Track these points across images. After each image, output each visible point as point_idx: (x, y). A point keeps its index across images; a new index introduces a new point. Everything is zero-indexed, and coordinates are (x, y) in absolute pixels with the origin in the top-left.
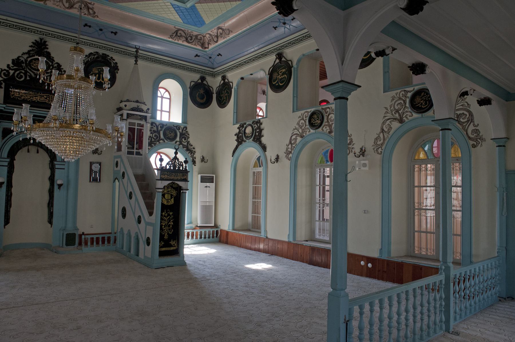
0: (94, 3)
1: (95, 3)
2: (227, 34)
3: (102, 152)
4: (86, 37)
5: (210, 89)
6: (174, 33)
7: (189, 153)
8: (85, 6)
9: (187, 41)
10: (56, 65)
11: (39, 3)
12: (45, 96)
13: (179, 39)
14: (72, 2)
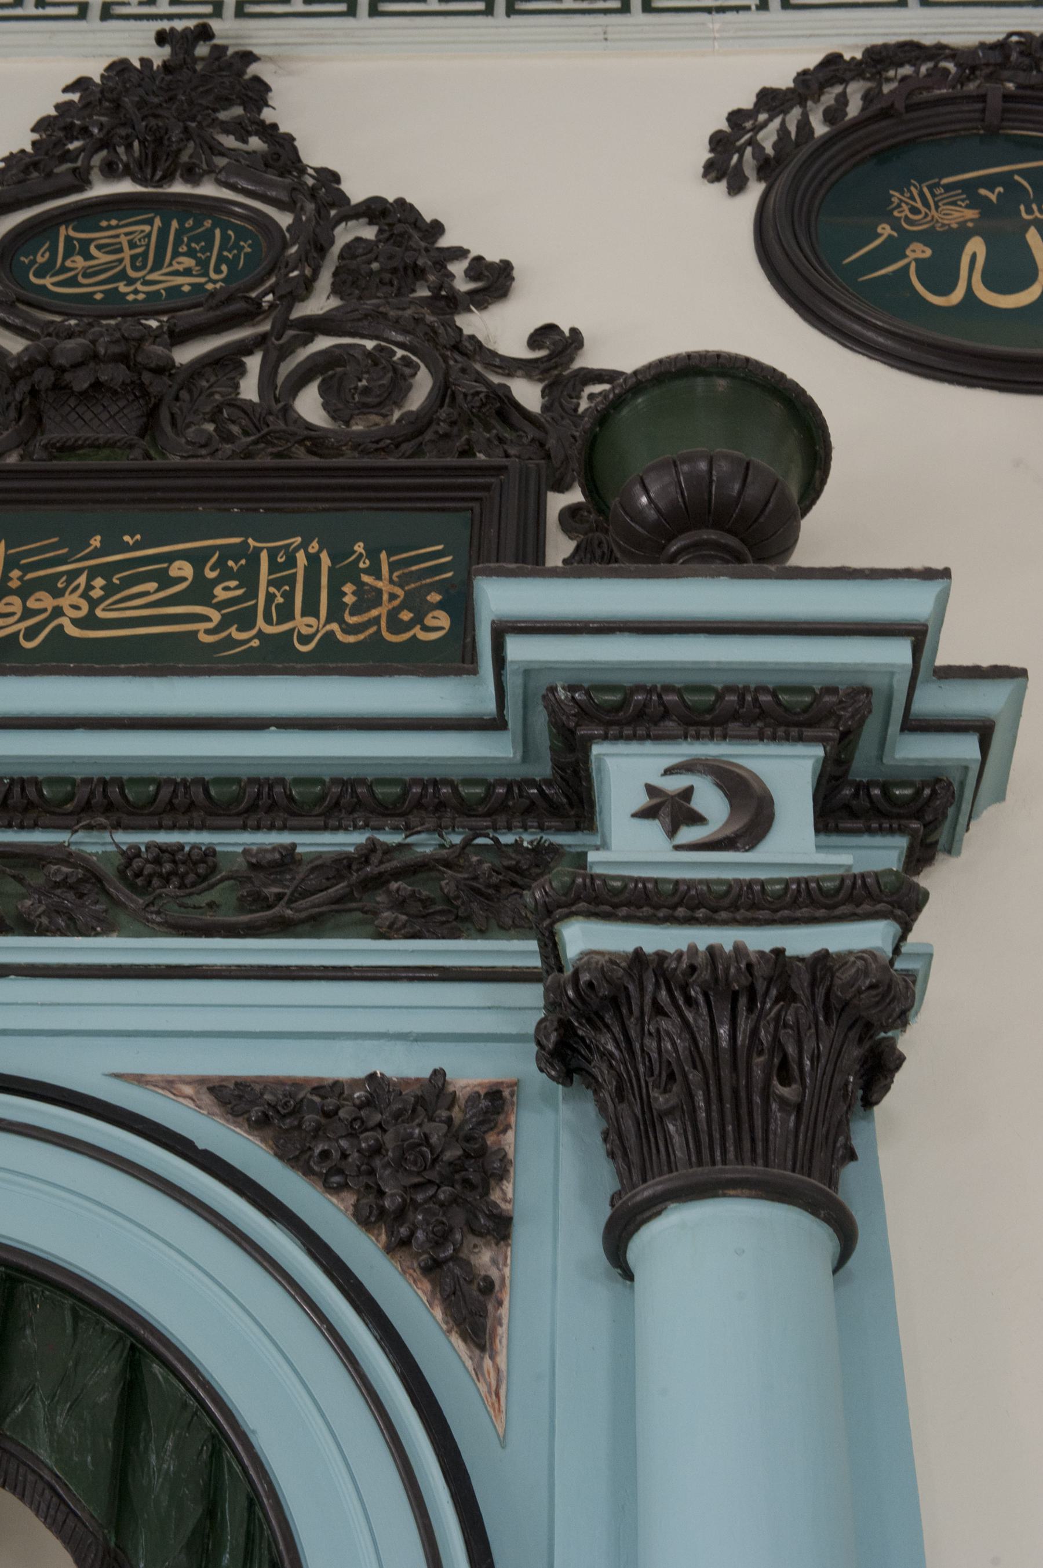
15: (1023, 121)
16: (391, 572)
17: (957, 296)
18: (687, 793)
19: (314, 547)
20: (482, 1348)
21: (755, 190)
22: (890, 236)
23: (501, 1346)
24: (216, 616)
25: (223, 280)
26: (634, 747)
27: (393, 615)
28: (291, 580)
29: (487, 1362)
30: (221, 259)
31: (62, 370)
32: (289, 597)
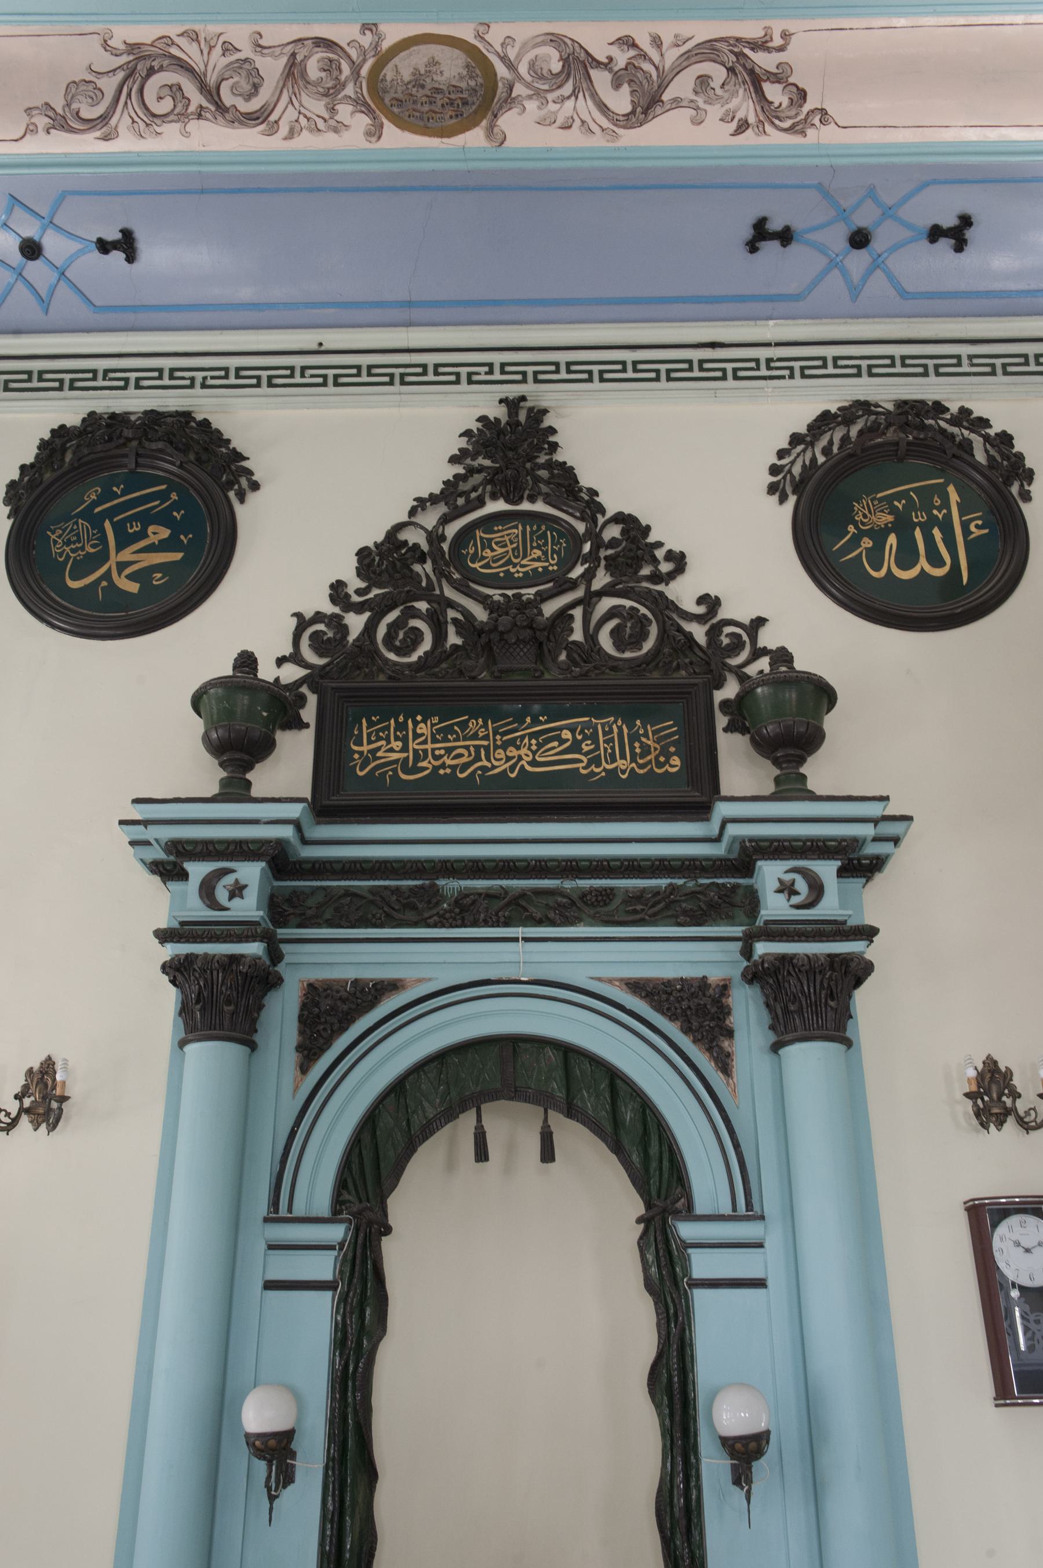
0: (786, 35)
1: (791, 26)
4: (771, 323)
8: (731, 70)
12: (566, 734)
15: (914, 456)
16: (653, 736)
17: (883, 572)
18: (793, 882)
19: (620, 723)
20: (729, 1076)
21: (792, 499)
22: (854, 533)
23: (734, 1075)
24: (585, 759)
25: (556, 564)
26: (773, 862)
27: (657, 758)
28: (612, 740)
29: (731, 1080)
30: (553, 551)
31: (502, 633)
32: (613, 748)
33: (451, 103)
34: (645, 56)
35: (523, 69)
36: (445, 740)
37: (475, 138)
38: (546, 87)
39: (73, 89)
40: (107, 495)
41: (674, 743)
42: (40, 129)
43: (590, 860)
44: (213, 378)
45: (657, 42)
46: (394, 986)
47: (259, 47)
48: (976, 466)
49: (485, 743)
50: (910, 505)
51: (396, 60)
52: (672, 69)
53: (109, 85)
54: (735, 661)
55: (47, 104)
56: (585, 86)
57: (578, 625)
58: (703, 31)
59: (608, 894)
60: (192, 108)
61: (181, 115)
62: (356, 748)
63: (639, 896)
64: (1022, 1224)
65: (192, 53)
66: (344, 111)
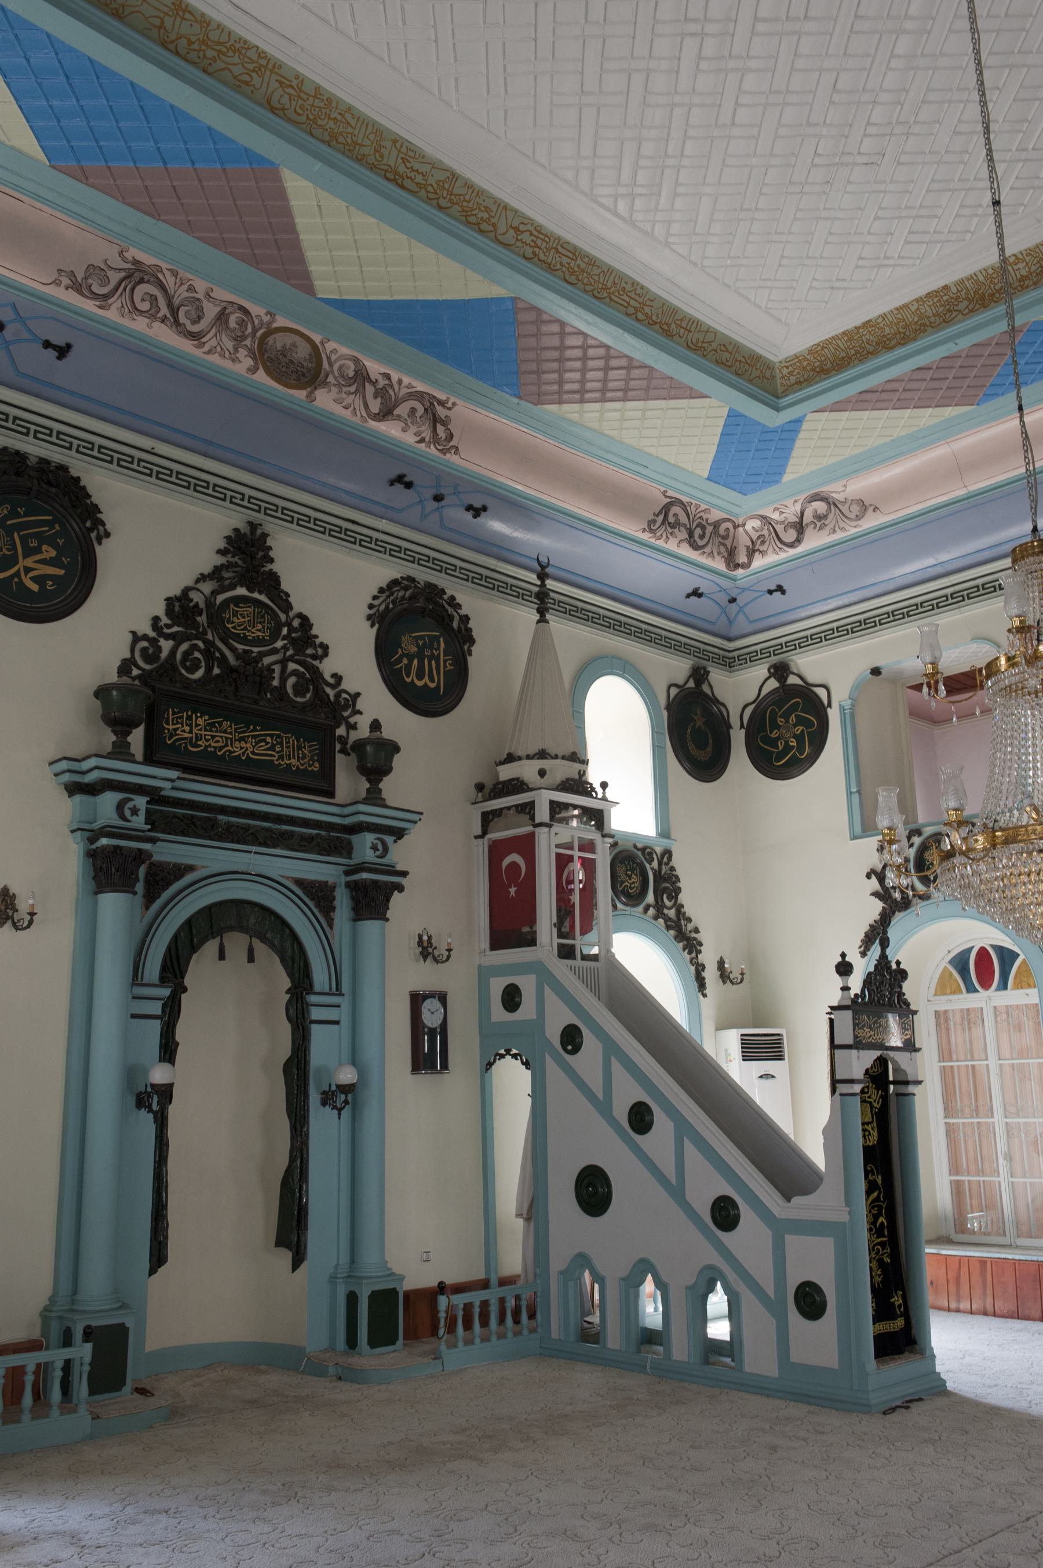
0: (454, 404)
1: (458, 402)
2: (852, 516)
3: (34, 917)
4: (384, 521)
5: (720, 711)
6: (660, 512)
7: (684, 950)
8: (426, 410)
9: (692, 540)
10: (296, 623)
11: (292, 395)
12: (269, 739)
13: (671, 534)
14: (390, 398)
21: (377, 626)
27: (309, 761)
33: (297, 372)
34: (392, 386)
35: (336, 367)
36: (211, 730)
37: (301, 394)
38: (343, 383)
39: (91, 269)
40: (13, 514)
41: (316, 754)
42: (63, 285)
43: (287, 816)
44: (84, 447)
45: (400, 382)
46: (191, 868)
47: (208, 295)
48: (453, 629)
49: (230, 736)
50: (424, 644)
51: (276, 335)
52: (402, 398)
53: (115, 277)
54: (346, 714)
55: (72, 272)
56: (361, 391)
57: (277, 675)
58: (420, 387)
59: (292, 834)
60: (160, 315)
61: (152, 315)
62: (166, 726)
63: (303, 837)
64: (432, 1002)
65: (170, 281)
66: (242, 353)
